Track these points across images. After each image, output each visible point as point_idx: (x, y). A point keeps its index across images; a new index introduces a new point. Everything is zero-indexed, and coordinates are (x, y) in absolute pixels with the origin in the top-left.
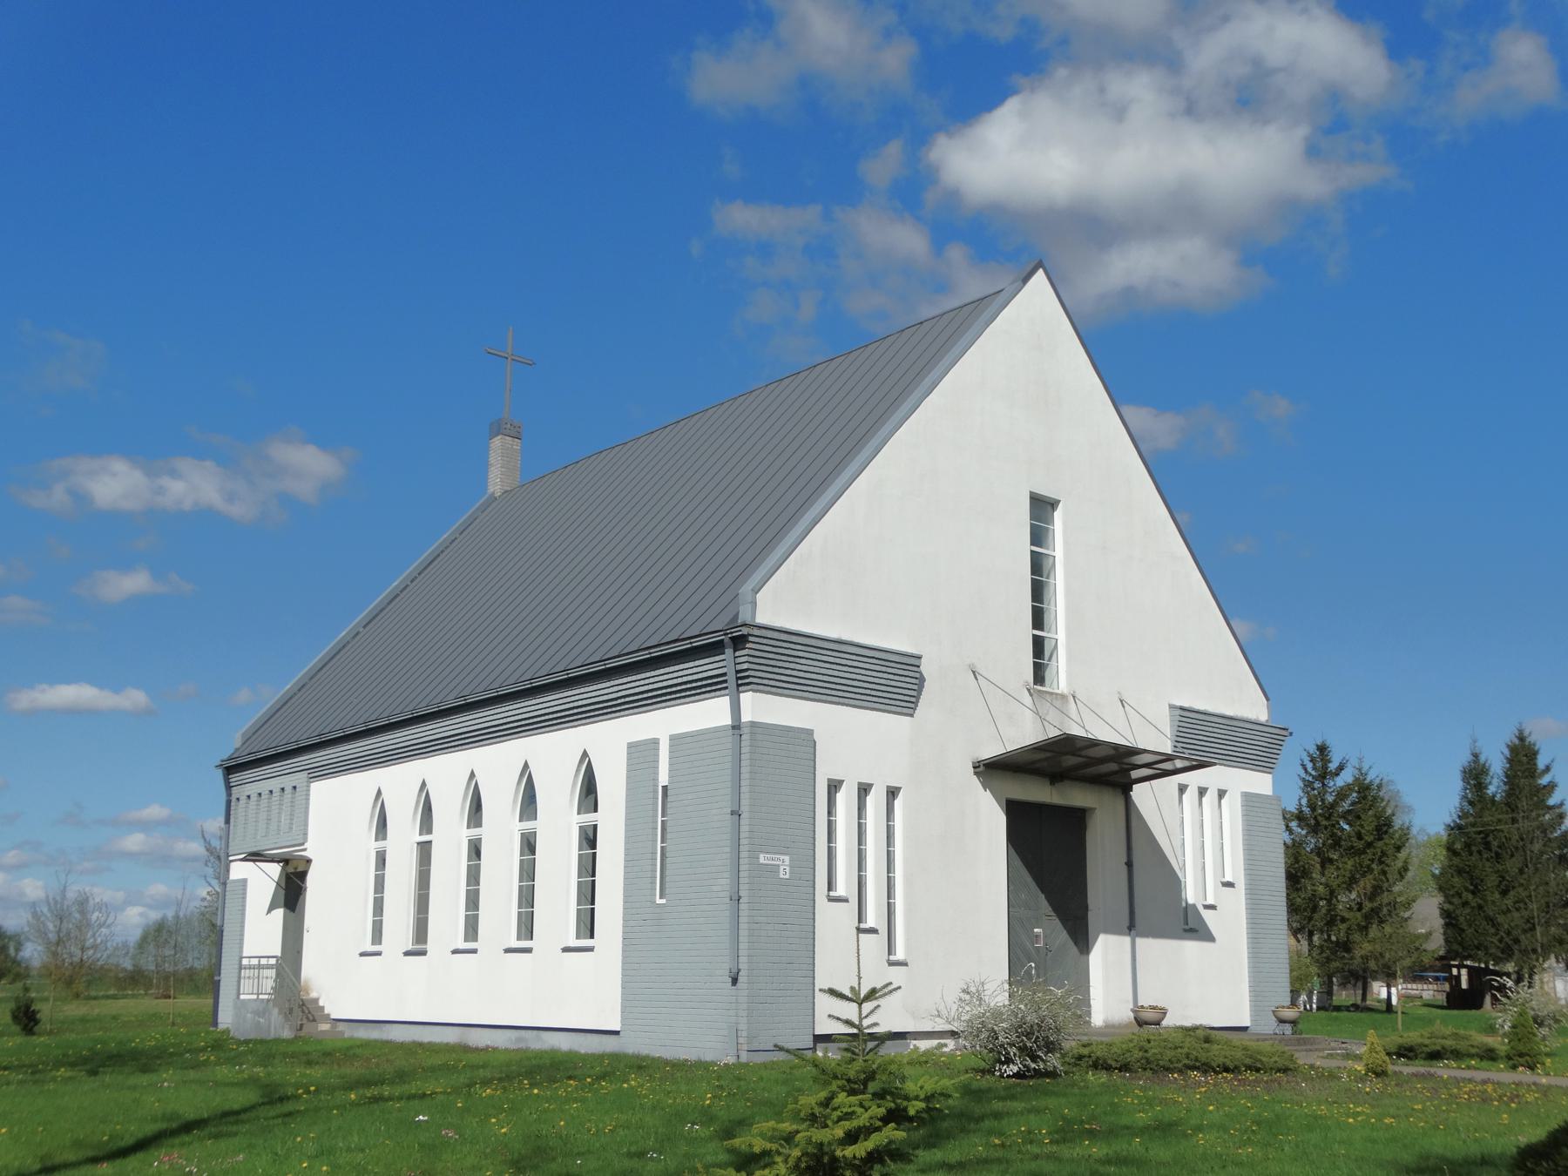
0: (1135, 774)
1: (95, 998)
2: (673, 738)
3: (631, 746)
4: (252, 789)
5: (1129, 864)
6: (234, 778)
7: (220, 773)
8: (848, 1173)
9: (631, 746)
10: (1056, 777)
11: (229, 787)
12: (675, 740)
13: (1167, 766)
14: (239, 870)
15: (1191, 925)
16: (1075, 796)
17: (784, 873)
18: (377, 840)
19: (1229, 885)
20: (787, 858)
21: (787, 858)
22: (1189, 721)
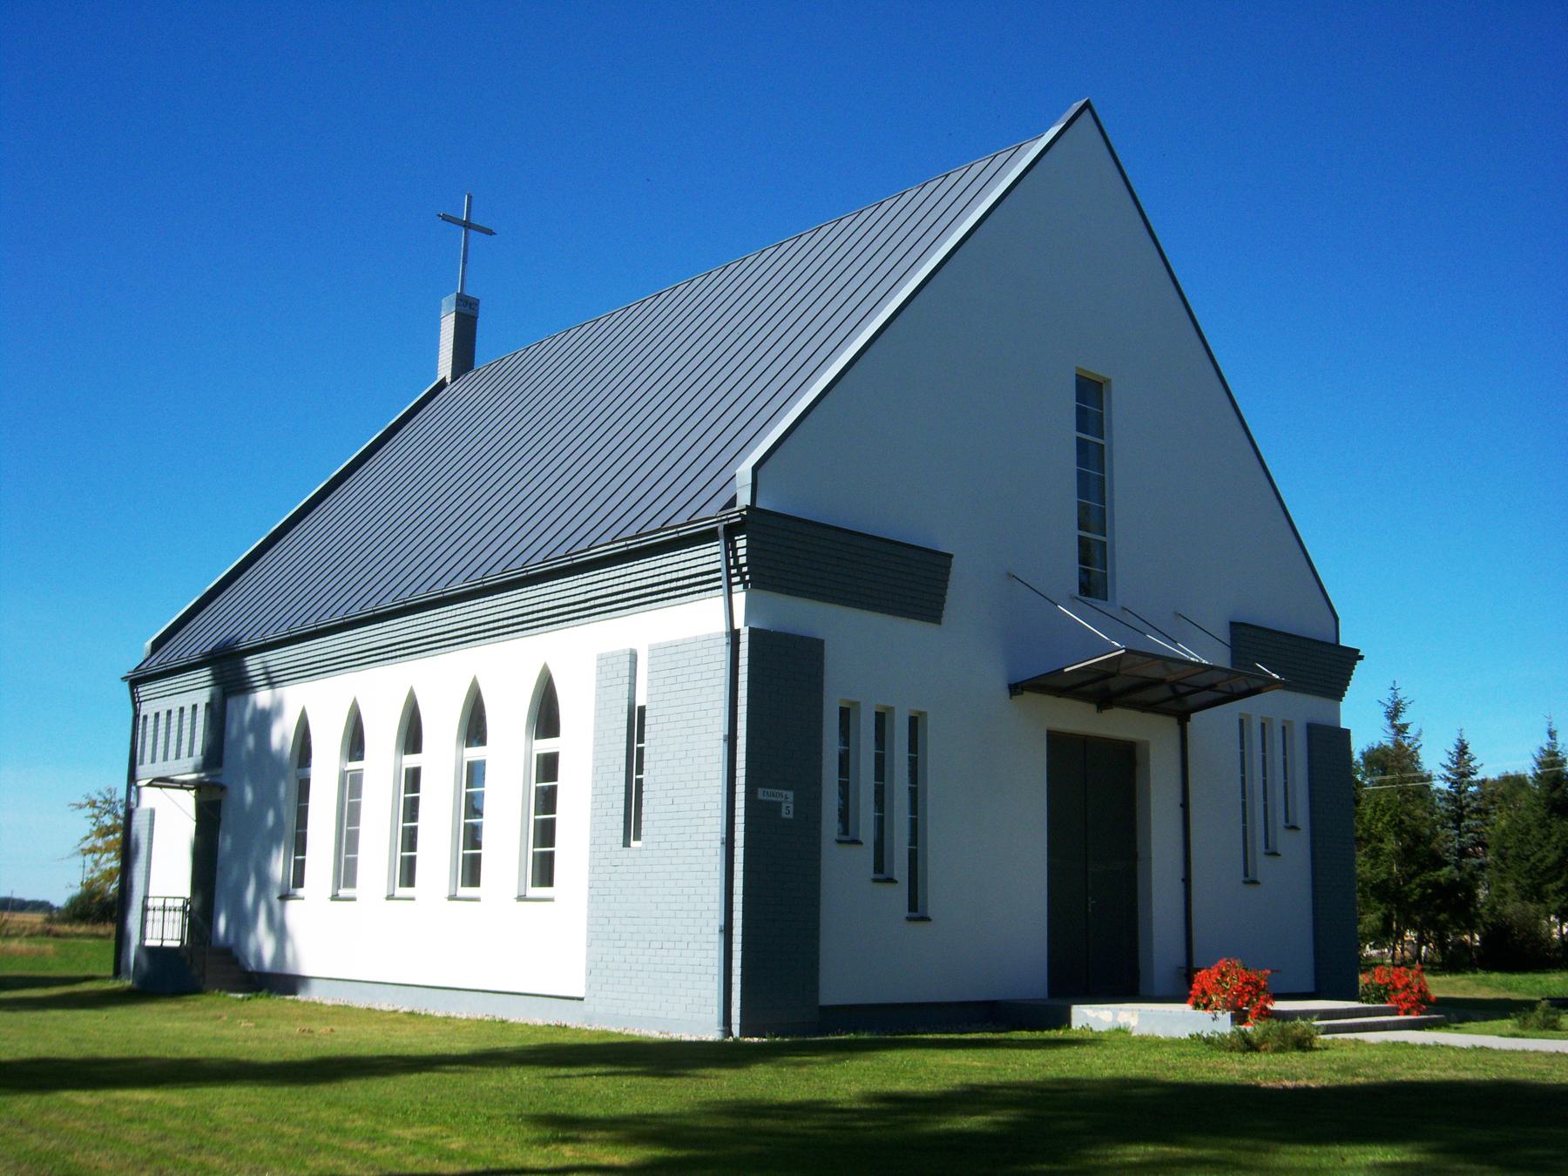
0: (1192, 700)
1: (57, 935)
2: (652, 649)
3: (601, 658)
4: (162, 706)
5: (1185, 805)
6: (144, 690)
7: (126, 685)
8: (1565, 930)
9: (601, 658)
10: (1105, 700)
11: (136, 703)
12: (656, 651)
13: (674, 650)
14: (151, 798)
15: (1251, 876)
16: (1118, 724)
17: (787, 811)
18: (483, 763)
19: (1294, 828)
20: (790, 794)
21: (790, 794)
22: (1244, 636)
